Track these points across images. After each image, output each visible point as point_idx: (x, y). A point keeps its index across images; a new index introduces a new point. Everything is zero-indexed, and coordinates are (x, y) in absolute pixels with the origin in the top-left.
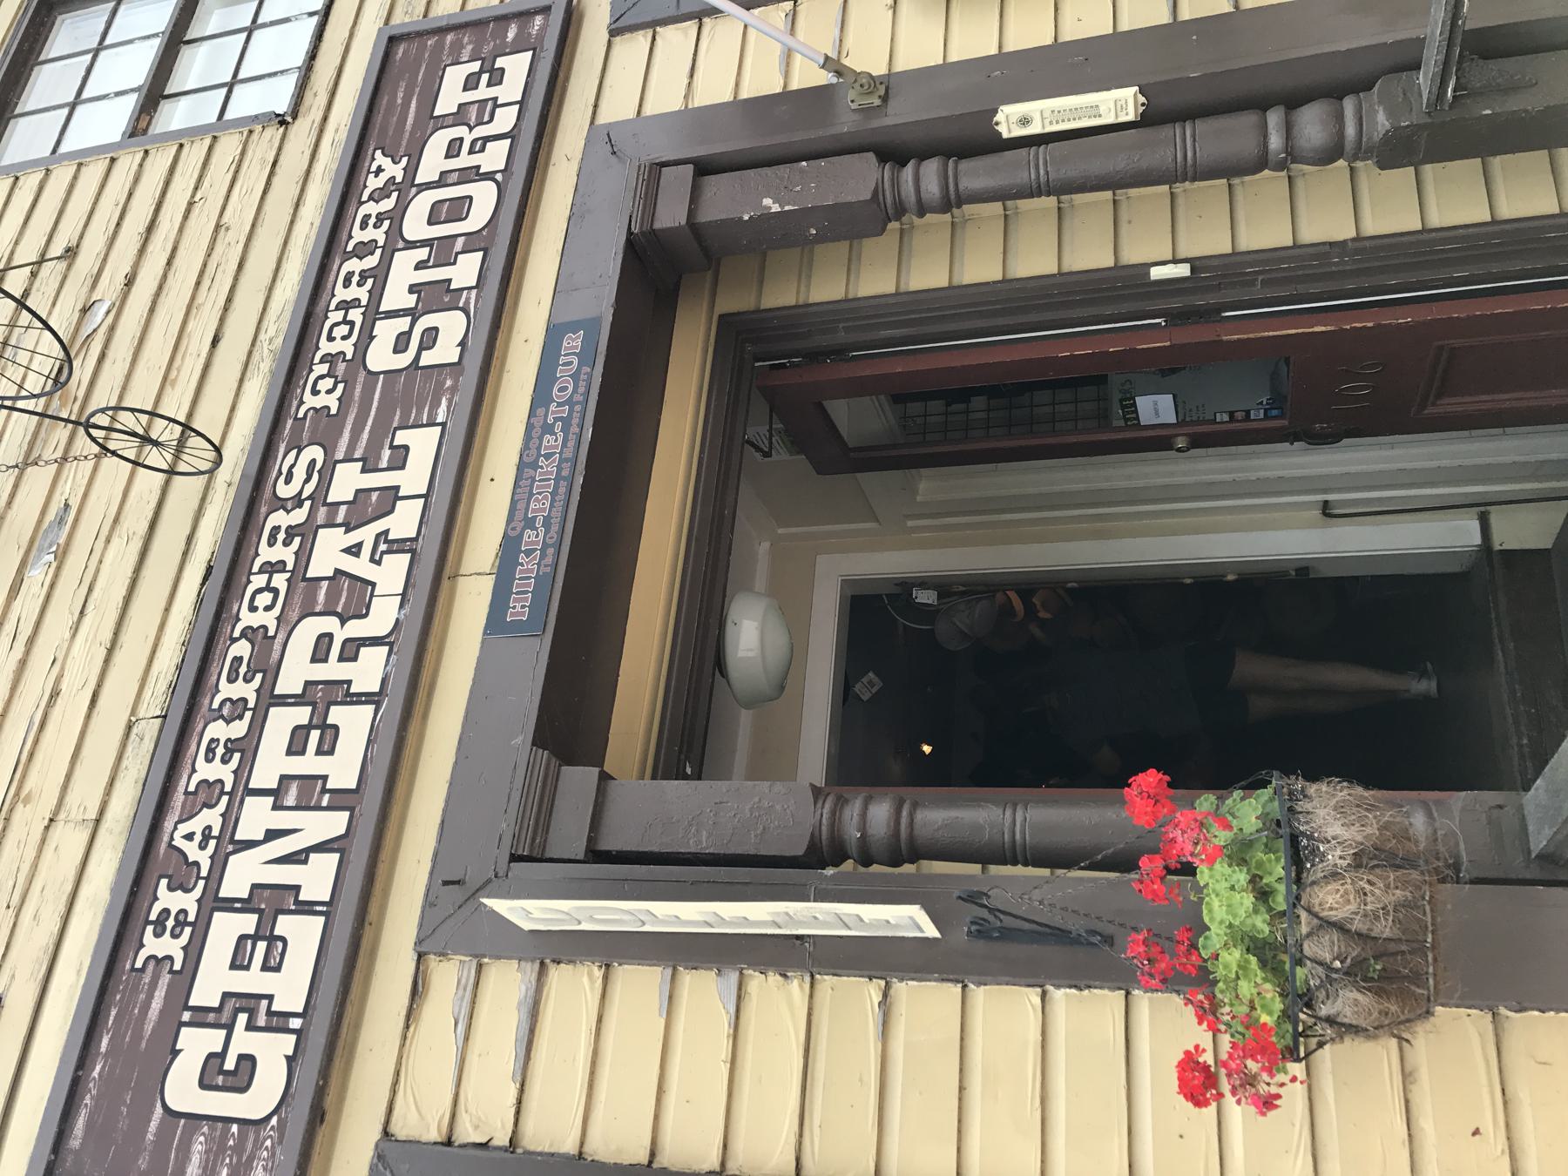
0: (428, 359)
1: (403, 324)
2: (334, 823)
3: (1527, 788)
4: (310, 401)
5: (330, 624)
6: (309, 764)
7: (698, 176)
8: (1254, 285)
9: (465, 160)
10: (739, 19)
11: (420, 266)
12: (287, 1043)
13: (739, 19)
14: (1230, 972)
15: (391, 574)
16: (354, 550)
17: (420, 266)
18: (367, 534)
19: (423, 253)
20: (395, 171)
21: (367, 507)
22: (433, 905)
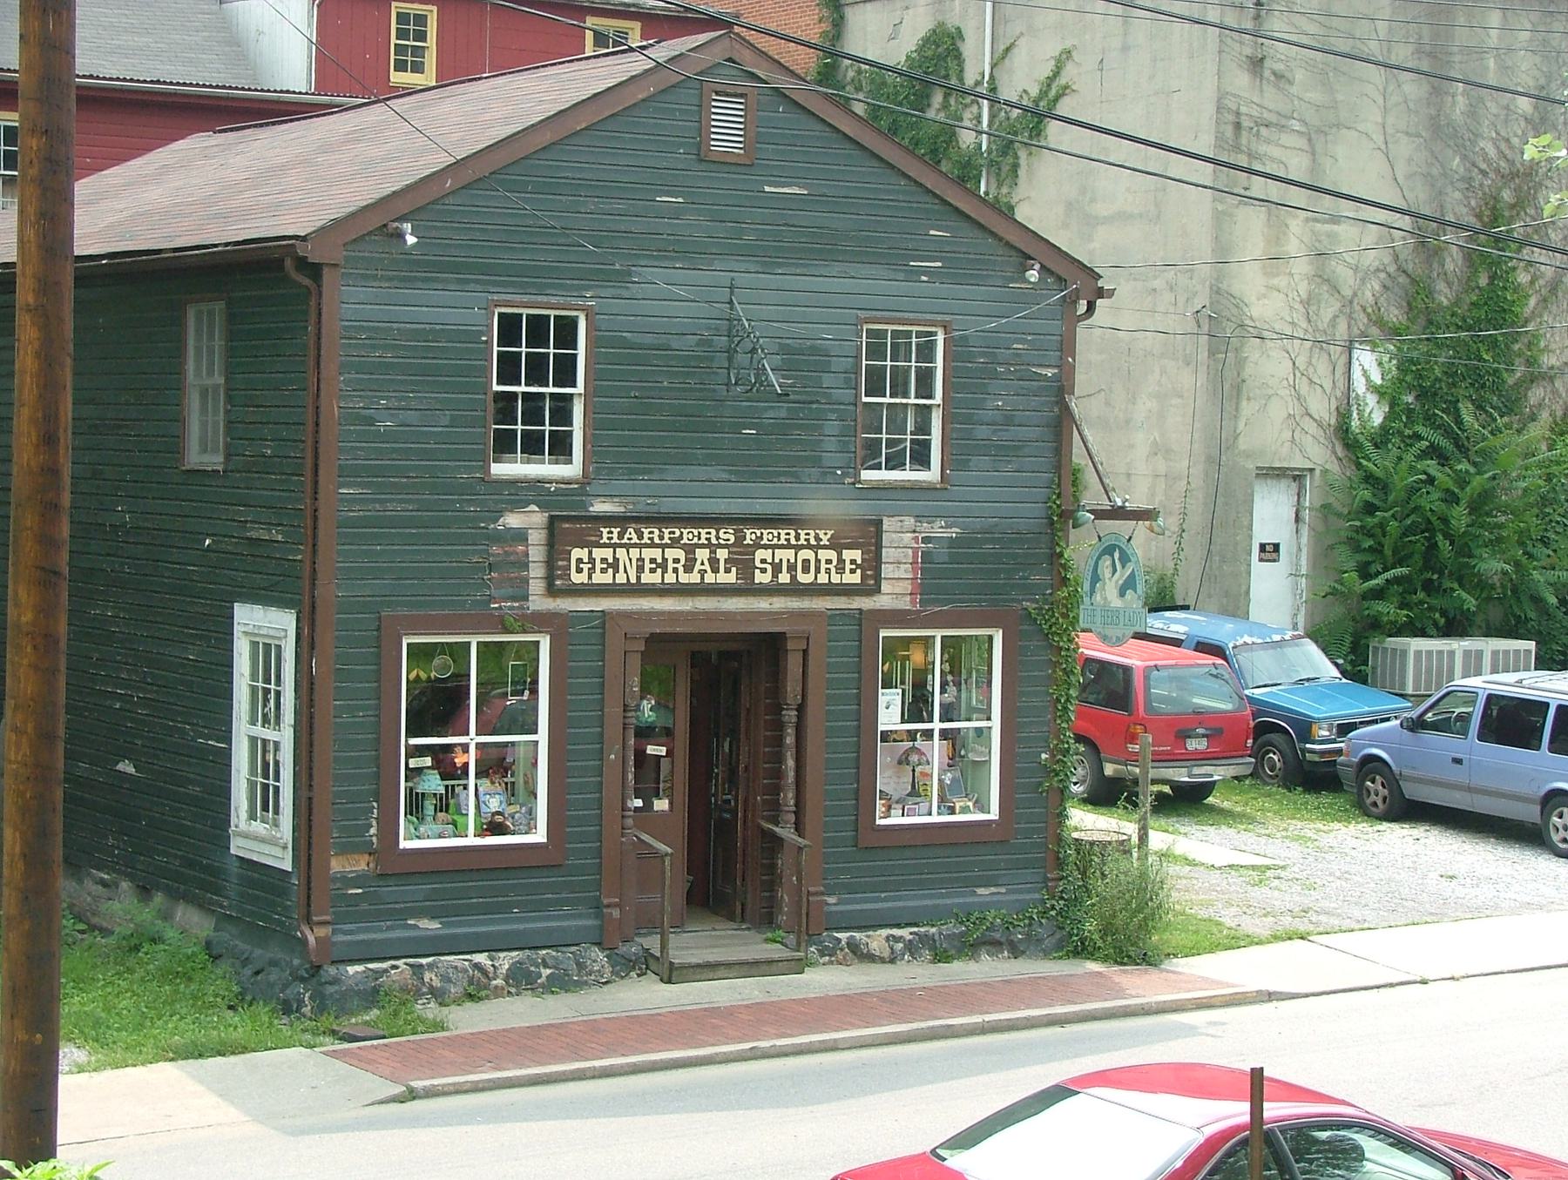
0: (757, 571)
1: (770, 560)
2: (633, 580)
3: (1127, 670)
4: (748, 532)
5: (683, 562)
6: (648, 566)
7: (698, 660)
8: (278, 787)
9: (823, 566)
10: (808, 644)
11: (788, 560)
12: (586, 582)
13: (808, 644)
14: (1403, 550)
15: (695, 578)
16: (702, 564)
17: (788, 560)
18: (707, 567)
19: (792, 561)
20: (825, 542)
21: (714, 562)
22: (534, 659)
